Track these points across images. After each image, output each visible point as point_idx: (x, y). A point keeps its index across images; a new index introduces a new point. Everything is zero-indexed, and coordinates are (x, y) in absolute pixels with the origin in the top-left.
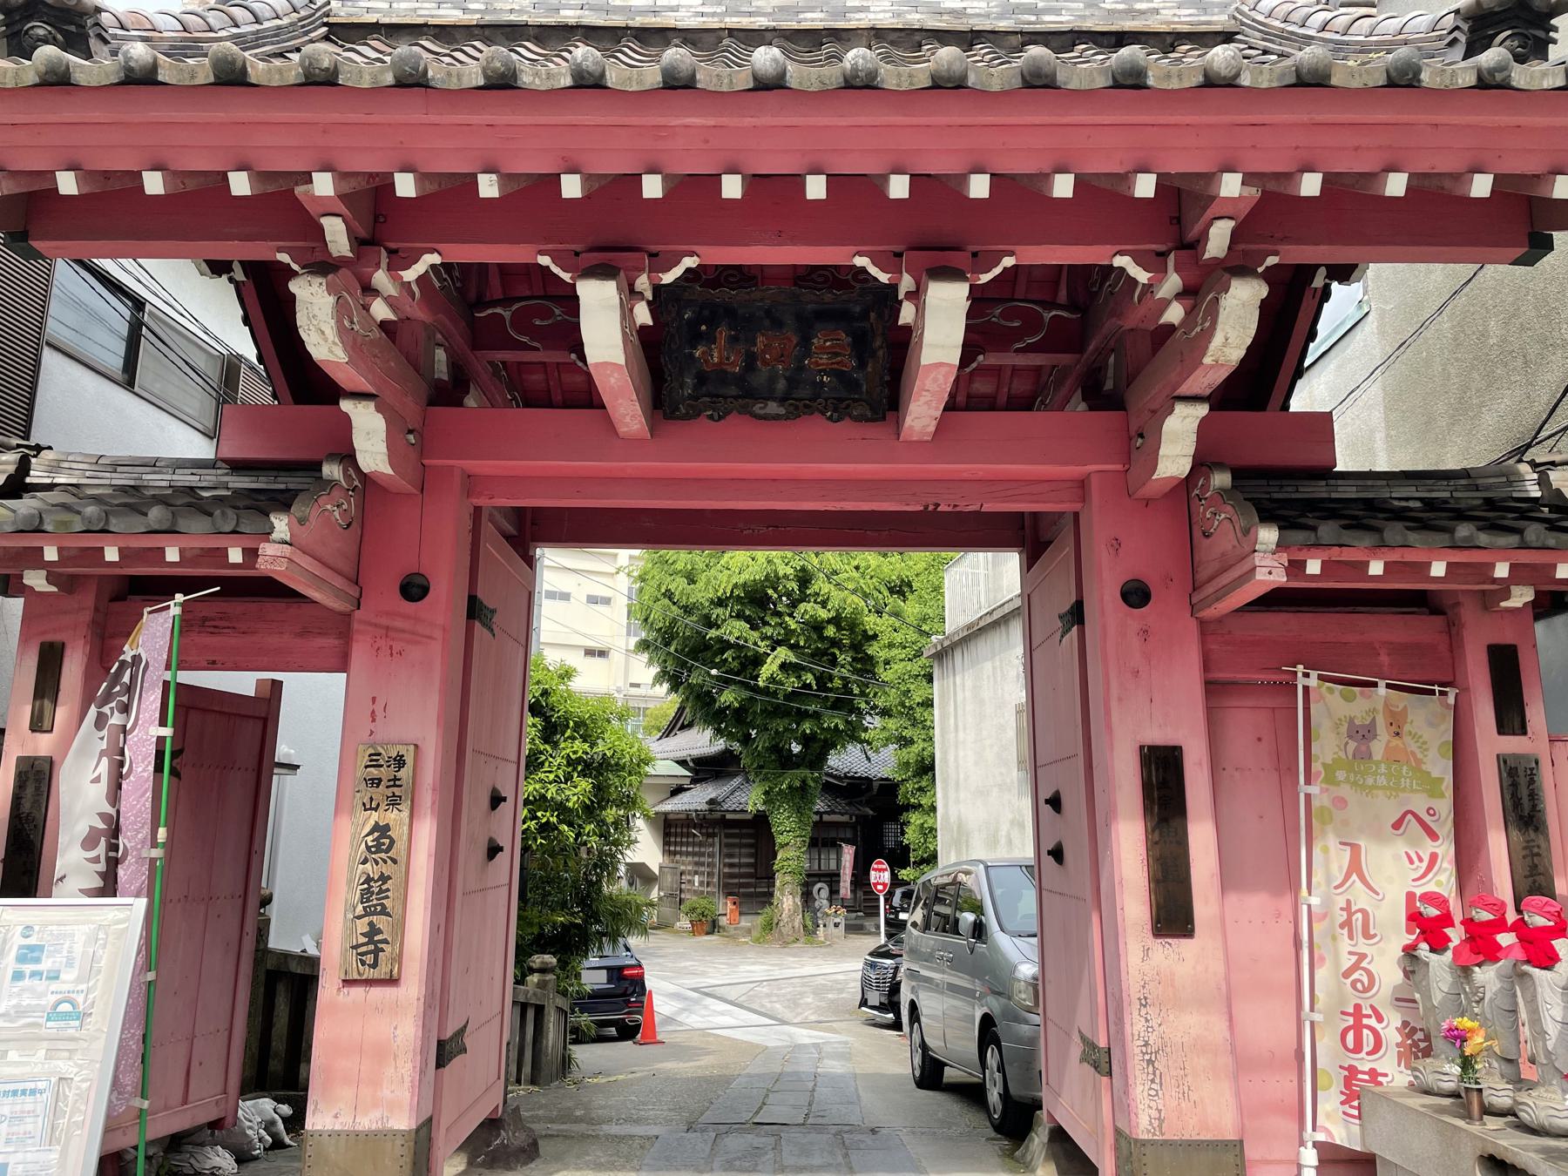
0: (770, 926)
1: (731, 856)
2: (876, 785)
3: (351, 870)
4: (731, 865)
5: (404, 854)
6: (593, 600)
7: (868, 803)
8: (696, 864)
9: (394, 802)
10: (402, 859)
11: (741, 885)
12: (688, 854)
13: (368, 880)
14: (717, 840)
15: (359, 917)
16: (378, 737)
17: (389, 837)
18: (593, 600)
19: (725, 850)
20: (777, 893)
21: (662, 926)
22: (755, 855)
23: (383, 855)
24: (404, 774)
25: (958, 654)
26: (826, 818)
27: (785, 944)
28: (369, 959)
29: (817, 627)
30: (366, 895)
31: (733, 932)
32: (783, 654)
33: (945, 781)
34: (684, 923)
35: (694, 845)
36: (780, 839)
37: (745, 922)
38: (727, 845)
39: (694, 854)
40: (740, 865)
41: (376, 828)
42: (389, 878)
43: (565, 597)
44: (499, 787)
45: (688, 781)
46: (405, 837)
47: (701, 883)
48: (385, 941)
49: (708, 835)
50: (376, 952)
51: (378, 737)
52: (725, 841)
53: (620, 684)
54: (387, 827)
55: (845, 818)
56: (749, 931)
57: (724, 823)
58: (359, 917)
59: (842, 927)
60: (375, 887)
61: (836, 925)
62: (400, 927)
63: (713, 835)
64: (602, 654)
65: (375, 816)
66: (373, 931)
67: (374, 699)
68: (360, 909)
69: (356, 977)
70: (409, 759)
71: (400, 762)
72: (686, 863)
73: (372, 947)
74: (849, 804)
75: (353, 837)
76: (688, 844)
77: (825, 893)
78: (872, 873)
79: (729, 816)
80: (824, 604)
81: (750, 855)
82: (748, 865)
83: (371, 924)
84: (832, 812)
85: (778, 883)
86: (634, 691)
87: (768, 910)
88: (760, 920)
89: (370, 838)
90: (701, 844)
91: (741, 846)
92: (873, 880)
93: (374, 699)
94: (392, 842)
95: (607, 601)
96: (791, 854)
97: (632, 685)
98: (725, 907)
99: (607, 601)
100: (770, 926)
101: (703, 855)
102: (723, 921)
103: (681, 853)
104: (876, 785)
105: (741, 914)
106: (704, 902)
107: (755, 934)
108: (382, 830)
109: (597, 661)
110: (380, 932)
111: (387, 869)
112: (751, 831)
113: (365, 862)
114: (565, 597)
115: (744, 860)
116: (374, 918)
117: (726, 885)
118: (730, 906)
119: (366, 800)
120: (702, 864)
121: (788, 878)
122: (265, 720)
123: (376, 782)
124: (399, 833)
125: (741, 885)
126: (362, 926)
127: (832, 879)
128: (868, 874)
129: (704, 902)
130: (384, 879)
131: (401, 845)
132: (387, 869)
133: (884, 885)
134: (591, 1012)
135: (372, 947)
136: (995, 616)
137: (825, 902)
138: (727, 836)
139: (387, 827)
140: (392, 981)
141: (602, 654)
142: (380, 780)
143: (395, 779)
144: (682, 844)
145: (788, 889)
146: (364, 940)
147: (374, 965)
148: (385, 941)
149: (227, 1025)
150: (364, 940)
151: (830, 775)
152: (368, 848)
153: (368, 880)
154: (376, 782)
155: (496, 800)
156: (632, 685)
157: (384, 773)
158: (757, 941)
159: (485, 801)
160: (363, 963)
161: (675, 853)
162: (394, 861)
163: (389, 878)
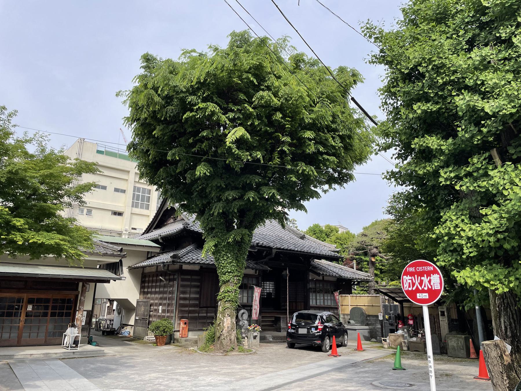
0: (212, 339)
1: (184, 293)
2: (274, 251)
4: (185, 299)
6: (116, 190)
7: (266, 264)
8: (161, 299)
11: (190, 312)
12: (156, 293)
14: (176, 283)
18: (116, 190)
19: (181, 289)
20: (219, 315)
21: (136, 339)
22: (200, 293)
27: (226, 352)
29: (268, 110)
31: (184, 343)
32: (240, 132)
34: (151, 337)
35: (160, 287)
36: (223, 278)
37: (192, 335)
38: (183, 286)
39: (160, 293)
40: (190, 299)
43: (104, 188)
45: (158, 251)
47: (163, 311)
49: (170, 280)
52: (181, 283)
53: (127, 228)
56: (196, 342)
57: (181, 272)
59: (258, 338)
61: (255, 337)
63: (174, 280)
64: (120, 214)
72: (154, 299)
74: (256, 264)
76: (156, 287)
77: (246, 316)
79: (185, 267)
80: (276, 95)
81: (196, 293)
82: (195, 299)
85: (220, 309)
86: (133, 231)
87: (211, 329)
88: (204, 334)
90: (165, 286)
91: (191, 286)
95: (124, 191)
96: (229, 289)
97: (133, 229)
98: (179, 327)
99: (124, 191)
100: (212, 339)
101: (165, 293)
102: (177, 335)
103: (151, 293)
104: (274, 251)
105: (189, 330)
106: (165, 323)
107: (201, 344)
109: (117, 217)
114: (104, 188)
115: (193, 296)
117: (181, 311)
118: (182, 325)
120: (165, 299)
121: (228, 305)
125: (190, 312)
127: (249, 307)
129: (165, 323)
134: (316, 192)
137: (246, 322)
138: (183, 280)
141: (120, 214)
144: (152, 287)
145: (228, 312)
156: (133, 229)
158: (204, 349)
161: (148, 293)
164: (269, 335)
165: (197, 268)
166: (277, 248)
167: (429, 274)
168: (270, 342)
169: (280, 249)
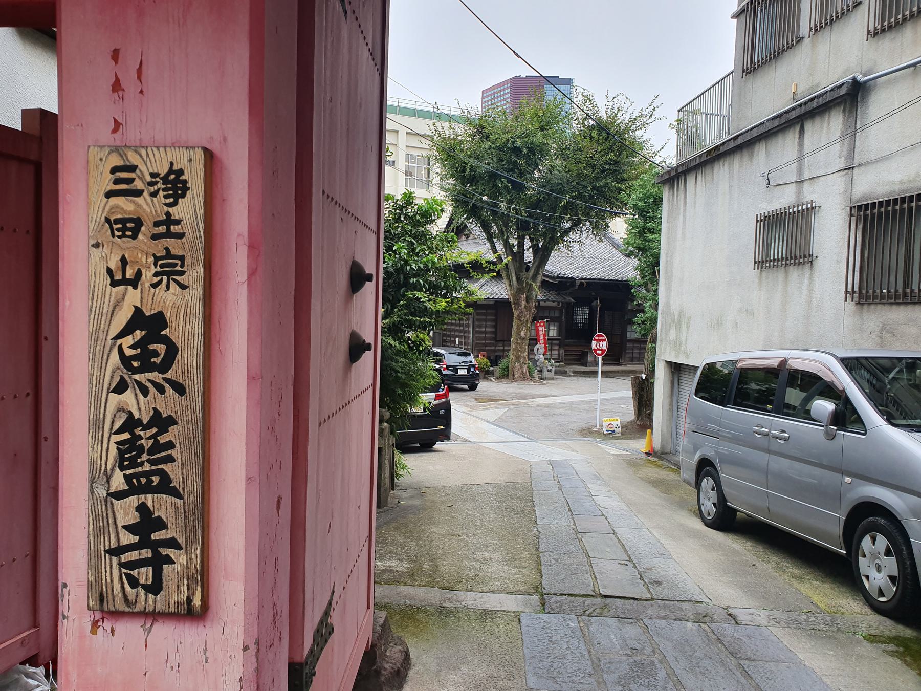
1: (480, 327)
2: (578, 282)
3: (96, 400)
5: (197, 375)
7: (570, 295)
9: (170, 269)
10: (195, 385)
13: (131, 424)
15: (119, 495)
16: (131, 134)
17: (167, 341)
19: (477, 323)
22: (495, 327)
23: (155, 376)
24: (189, 210)
25: (691, 180)
26: (542, 304)
28: (145, 574)
30: (128, 454)
33: (669, 279)
40: (486, 332)
41: (138, 320)
42: (171, 421)
44: (358, 259)
46: (198, 341)
48: (173, 543)
50: (158, 562)
51: (131, 134)
54: (159, 320)
55: (555, 304)
58: (119, 495)
60: (146, 439)
62: (201, 517)
65: (133, 297)
66: (147, 523)
67: (115, 55)
68: (118, 481)
69: (121, 606)
70: (195, 177)
71: (175, 185)
73: (147, 553)
74: (558, 294)
75: (94, 337)
78: (594, 343)
83: (142, 509)
84: (547, 300)
89: (129, 340)
91: (486, 321)
92: (593, 347)
93: (115, 55)
94: (172, 350)
104: (578, 282)
108: (150, 325)
110: (161, 525)
111: (168, 403)
112: (493, 311)
113: (121, 388)
116: (149, 499)
119: (114, 263)
122: (38, 167)
123: (129, 227)
124: (185, 330)
126: (126, 512)
128: (591, 343)
130: (161, 422)
131: (189, 357)
132: (168, 403)
133: (603, 351)
135: (147, 553)
136: (740, 141)
139: (159, 320)
140: (193, 613)
142: (138, 222)
143: (169, 221)
146: (128, 538)
147: (155, 587)
148: (173, 543)
149: (28, 550)
150: (128, 538)
151: (547, 276)
152: (125, 360)
153: (131, 424)
154: (129, 227)
155: (358, 278)
157: (150, 207)
159: (342, 279)
160: (134, 582)
162: (180, 389)
163: (171, 421)
164: (569, 369)
165: (492, 302)
166: (582, 279)
167: (603, 341)
168: (570, 376)
169: (585, 279)
